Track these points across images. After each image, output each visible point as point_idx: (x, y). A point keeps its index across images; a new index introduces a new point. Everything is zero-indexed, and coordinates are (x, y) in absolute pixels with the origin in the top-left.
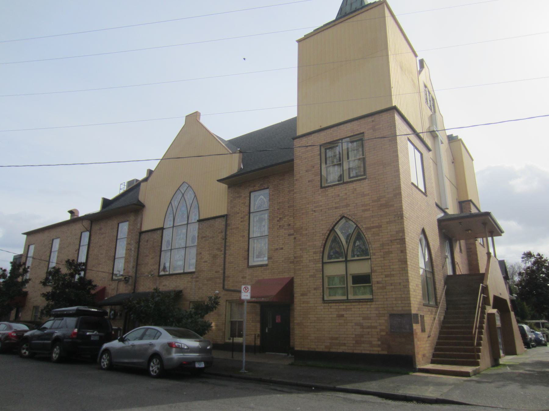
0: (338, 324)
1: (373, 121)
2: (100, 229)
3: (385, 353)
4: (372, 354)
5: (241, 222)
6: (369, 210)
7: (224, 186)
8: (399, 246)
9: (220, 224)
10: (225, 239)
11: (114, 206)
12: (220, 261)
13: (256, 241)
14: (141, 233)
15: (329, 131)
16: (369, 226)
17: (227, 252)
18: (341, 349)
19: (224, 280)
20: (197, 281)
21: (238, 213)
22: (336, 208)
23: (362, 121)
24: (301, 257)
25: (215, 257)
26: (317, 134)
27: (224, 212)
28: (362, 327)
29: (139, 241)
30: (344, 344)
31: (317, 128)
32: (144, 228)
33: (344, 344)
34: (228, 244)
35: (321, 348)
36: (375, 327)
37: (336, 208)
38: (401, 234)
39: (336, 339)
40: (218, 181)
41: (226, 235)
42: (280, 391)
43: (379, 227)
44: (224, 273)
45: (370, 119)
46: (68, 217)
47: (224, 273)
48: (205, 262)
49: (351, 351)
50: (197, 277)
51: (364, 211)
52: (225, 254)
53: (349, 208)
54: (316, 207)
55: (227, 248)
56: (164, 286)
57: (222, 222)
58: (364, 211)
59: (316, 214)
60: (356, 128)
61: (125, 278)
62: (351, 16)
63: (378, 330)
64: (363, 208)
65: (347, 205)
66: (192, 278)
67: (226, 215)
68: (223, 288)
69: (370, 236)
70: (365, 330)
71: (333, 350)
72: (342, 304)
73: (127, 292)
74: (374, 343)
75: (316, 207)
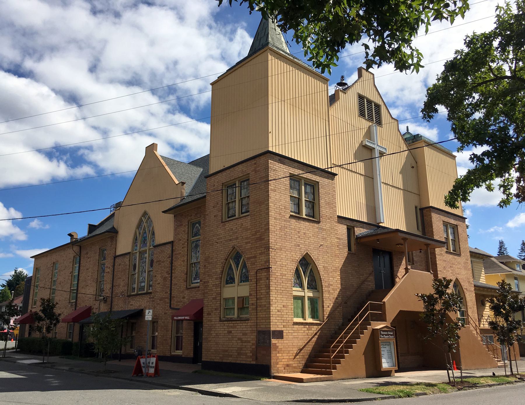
0: (228, 339)
1: (255, 164)
2: (87, 253)
3: (254, 363)
4: (247, 364)
5: (183, 248)
6: (249, 242)
7: (170, 217)
8: (266, 274)
9: (168, 248)
10: (172, 263)
11: (98, 232)
12: (168, 283)
13: (83, 291)
14: (116, 257)
15: (228, 171)
16: (249, 256)
17: (173, 275)
18: (230, 360)
19: (171, 301)
20: (153, 301)
21: (181, 240)
22: (230, 240)
23: (249, 163)
24: (208, 282)
25: (165, 279)
26: (220, 174)
27: (171, 239)
28: (242, 342)
29: (114, 265)
30: (231, 356)
31: (222, 168)
32: (118, 253)
33: (231, 356)
34: (173, 268)
35: (217, 359)
36: (249, 342)
37: (230, 240)
38: (267, 264)
39: (227, 351)
40: (163, 212)
41: (172, 259)
42: (150, 383)
43: (255, 257)
44: (171, 293)
45: (253, 162)
46: (68, 240)
47: (171, 293)
48: (159, 284)
49: (234, 362)
50: (153, 298)
51: (247, 243)
52: (171, 277)
53: (238, 240)
54: (218, 239)
55: (173, 271)
56: (131, 305)
57: (168, 248)
58: (247, 243)
59: (218, 245)
60: (238, 172)
61: (104, 298)
62: (261, 51)
63: (251, 344)
64: (246, 241)
65: (237, 238)
66: (150, 298)
67: (173, 242)
68: (170, 306)
69: (249, 265)
70: (243, 344)
71: (224, 361)
72: (231, 322)
73: (106, 310)
74: (248, 354)
75: (218, 239)
